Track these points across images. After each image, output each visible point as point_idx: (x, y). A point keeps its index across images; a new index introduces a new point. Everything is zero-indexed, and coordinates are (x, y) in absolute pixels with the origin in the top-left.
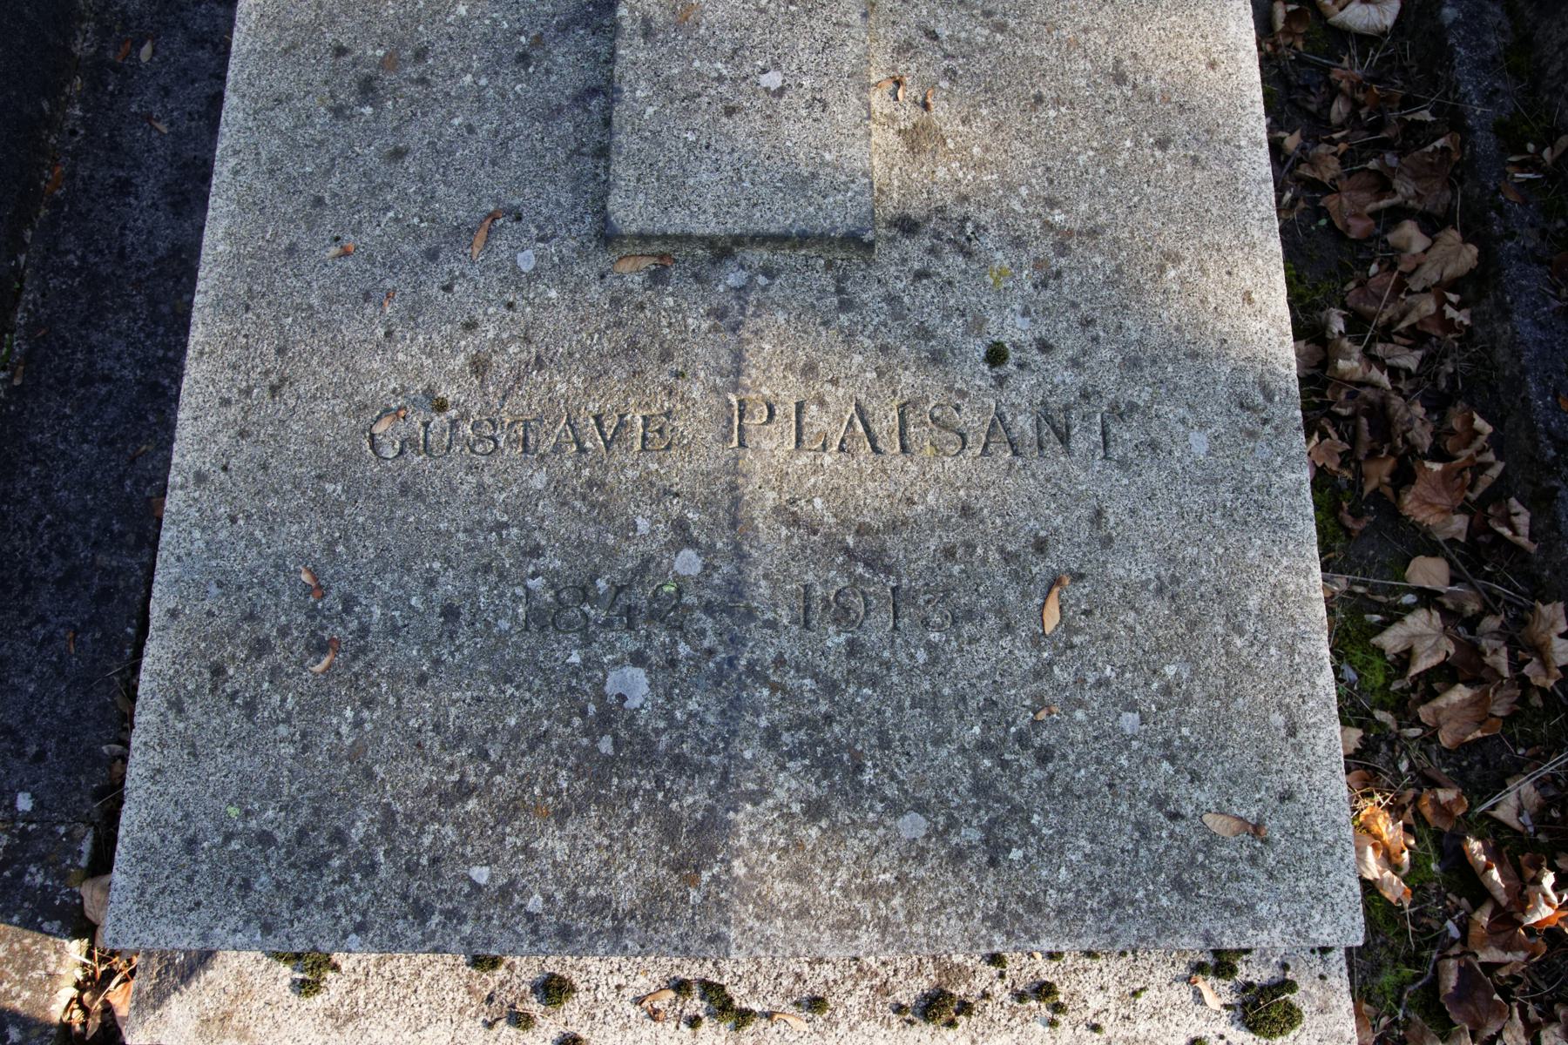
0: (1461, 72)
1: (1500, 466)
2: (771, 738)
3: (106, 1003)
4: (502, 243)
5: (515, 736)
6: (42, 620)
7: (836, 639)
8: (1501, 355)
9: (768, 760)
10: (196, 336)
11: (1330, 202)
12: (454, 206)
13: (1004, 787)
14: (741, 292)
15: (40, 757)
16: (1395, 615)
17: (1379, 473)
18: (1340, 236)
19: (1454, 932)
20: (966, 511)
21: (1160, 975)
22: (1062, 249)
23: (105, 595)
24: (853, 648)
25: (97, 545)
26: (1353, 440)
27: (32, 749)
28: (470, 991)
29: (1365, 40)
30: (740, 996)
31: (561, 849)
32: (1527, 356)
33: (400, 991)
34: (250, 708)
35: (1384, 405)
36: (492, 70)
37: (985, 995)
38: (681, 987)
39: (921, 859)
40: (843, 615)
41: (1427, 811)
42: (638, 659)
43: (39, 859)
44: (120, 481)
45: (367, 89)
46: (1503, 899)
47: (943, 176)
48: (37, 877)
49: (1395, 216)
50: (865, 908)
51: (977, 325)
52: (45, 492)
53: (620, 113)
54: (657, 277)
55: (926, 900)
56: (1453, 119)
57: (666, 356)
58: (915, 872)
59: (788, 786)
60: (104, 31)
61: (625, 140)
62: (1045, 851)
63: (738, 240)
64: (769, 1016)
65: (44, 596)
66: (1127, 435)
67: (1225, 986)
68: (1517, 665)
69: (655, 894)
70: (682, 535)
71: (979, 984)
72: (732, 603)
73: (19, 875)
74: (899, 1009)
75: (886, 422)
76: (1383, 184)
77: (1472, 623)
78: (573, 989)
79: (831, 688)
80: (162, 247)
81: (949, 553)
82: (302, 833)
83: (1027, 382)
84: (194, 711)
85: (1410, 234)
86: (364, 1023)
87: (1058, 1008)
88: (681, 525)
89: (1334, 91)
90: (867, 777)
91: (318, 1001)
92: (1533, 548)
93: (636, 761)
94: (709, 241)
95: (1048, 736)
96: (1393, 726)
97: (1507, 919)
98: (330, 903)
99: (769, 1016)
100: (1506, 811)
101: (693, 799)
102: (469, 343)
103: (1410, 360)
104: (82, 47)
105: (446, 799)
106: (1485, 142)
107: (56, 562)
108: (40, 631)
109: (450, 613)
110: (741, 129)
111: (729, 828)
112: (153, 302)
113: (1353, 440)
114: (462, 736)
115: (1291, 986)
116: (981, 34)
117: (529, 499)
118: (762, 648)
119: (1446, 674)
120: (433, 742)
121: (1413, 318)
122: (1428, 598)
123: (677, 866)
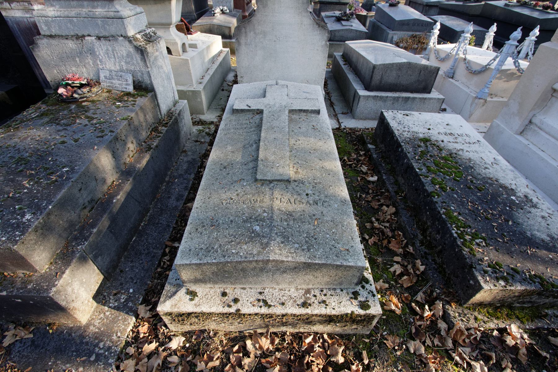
0: (387, 185)
1: (406, 241)
2: (276, 234)
3: (138, 330)
4: (242, 182)
5: (240, 235)
6: (142, 260)
7: (285, 223)
8: (402, 224)
9: (276, 236)
10: (198, 193)
11: (371, 204)
12: (235, 178)
13: (310, 242)
14: (273, 186)
15: (136, 283)
16: (392, 266)
17: (385, 242)
18: (374, 208)
19: (412, 321)
20: (303, 211)
21: (344, 299)
22: (316, 184)
23: (154, 256)
24: (288, 225)
25: (154, 248)
26: (379, 237)
27: (135, 281)
28: (221, 301)
29: (373, 182)
30: (269, 302)
31: (246, 247)
32: (406, 222)
33: (208, 300)
34: (201, 233)
35: (383, 230)
36: (241, 166)
37: (313, 303)
38: (259, 300)
39: (298, 249)
40: (286, 221)
41: (403, 299)
42: (258, 225)
43: (132, 301)
44: (160, 239)
45: (225, 168)
46: (420, 314)
47: (300, 176)
48: (130, 304)
49: (382, 205)
50: (290, 255)
51: (305, 191)
52: (147, 240)
53: (258, 168)
54: (262, 185)
55: (299, 255)
56: (388, 191)
57: (263, 193)
58: (297, 251)
59: (279, 239)
60: (170, 177)
61: (259, 170)
62: (316, 250)
63: (273, 180)
64: (274, 306)
65: (143, 256)
66: (326, 204)
67: (356, 301)
68: (414, 272)
69: (259, 252)
70: (265, 211)
71: (312, 300)
72: (271, 219)
73: (127, 304)
74: (298, 305)
75: (292, 201)
76: (379, 201)
77: (407, 266)
78: (239, 300)
79: (285, 229)
80: (174, 206)
81: (301, 215)
82: (207, 248)
83: (311, 198)
84: (193, 234)
85: (385, 208)
86: (201, 306)
87: (327, 305)
88: (264, 210)
89: (369, 189)
90: (290, 239)
91: (193, 302)
92: (414, 253)
93: (257, 236)
94: (269, 181)
95: (316, 237)
96: (394, 284)
97: (422, 318)
98: (211, 256)
99: (274, 306)
100: (419, 299)
101: (265, 240)
102: (237, 192)
103: (387, 225)
104: (167, 179)
105: (229, 243)
106: (393, 194)
107: (146, 251)
108: (141, 262)
109: (232, 221)
110: (274, 170)
111: (271, 244)
112: (171, 213)
113: (379, 237)
114: (232, 235)
115: (368, 301)
116: (304, 163)
117: (244, 208)
118: (275, 223)
119: (401, 275)
120: (228, 236)
121: (387, 219)
122: (398, 263)
123: (262, 248)
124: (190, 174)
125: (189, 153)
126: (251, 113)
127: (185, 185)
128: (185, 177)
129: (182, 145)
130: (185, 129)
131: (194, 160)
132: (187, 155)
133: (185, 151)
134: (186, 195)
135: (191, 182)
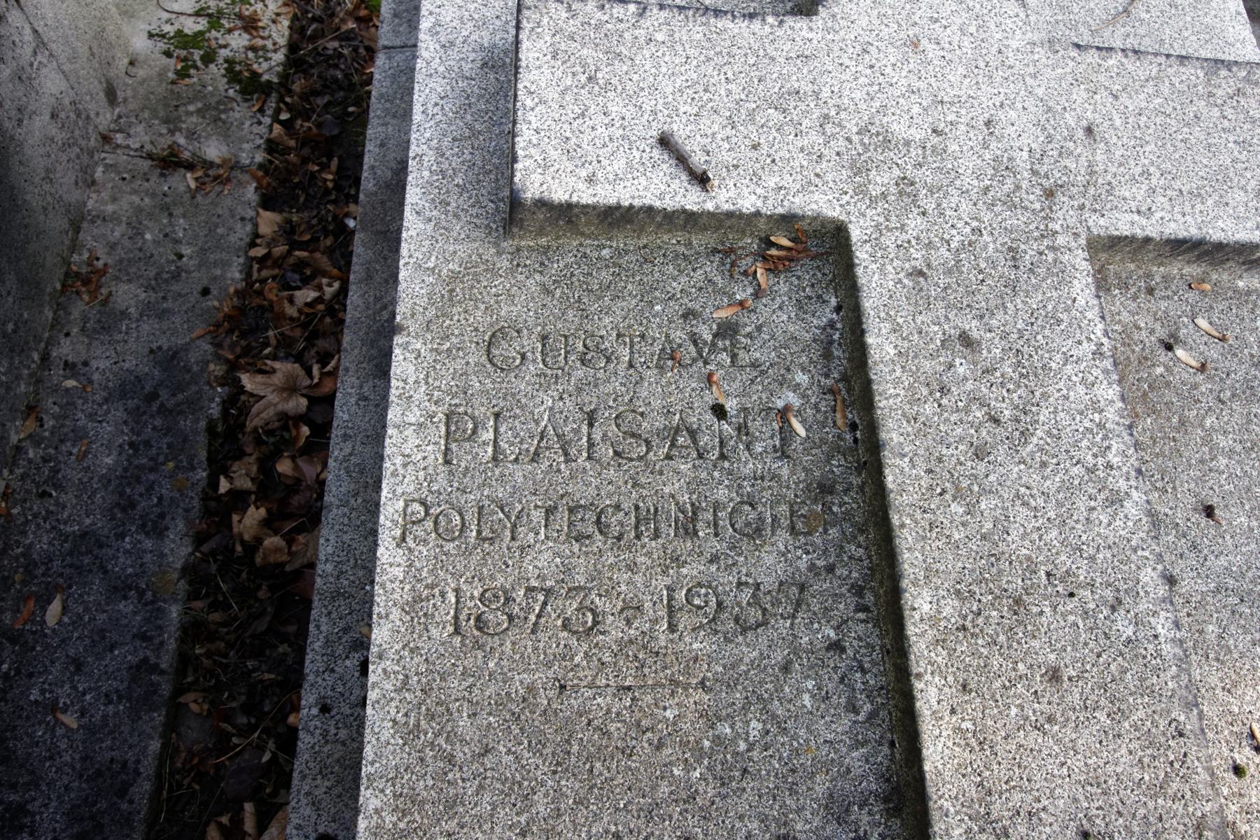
124: (157, 530)
125: (127, 295)
126: (700, 241)
127: (126, 655)
128: (123, 565)
129: (57, 223)
130: (52, 83)
131: (169, 360)
132: (107, 323)
133: (88, 280)
134: (148, 767)
135: (174, 611)
